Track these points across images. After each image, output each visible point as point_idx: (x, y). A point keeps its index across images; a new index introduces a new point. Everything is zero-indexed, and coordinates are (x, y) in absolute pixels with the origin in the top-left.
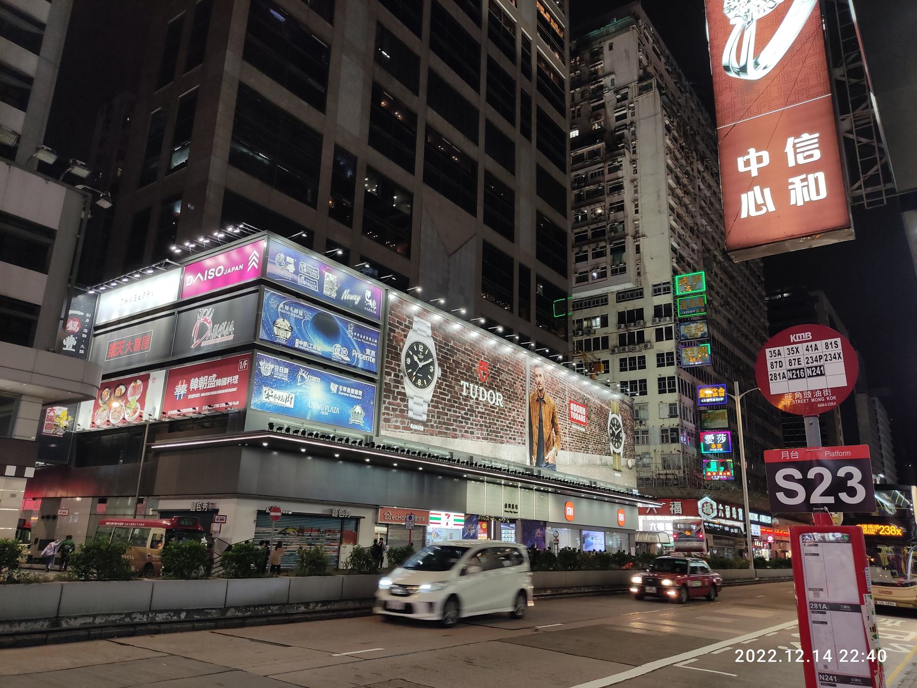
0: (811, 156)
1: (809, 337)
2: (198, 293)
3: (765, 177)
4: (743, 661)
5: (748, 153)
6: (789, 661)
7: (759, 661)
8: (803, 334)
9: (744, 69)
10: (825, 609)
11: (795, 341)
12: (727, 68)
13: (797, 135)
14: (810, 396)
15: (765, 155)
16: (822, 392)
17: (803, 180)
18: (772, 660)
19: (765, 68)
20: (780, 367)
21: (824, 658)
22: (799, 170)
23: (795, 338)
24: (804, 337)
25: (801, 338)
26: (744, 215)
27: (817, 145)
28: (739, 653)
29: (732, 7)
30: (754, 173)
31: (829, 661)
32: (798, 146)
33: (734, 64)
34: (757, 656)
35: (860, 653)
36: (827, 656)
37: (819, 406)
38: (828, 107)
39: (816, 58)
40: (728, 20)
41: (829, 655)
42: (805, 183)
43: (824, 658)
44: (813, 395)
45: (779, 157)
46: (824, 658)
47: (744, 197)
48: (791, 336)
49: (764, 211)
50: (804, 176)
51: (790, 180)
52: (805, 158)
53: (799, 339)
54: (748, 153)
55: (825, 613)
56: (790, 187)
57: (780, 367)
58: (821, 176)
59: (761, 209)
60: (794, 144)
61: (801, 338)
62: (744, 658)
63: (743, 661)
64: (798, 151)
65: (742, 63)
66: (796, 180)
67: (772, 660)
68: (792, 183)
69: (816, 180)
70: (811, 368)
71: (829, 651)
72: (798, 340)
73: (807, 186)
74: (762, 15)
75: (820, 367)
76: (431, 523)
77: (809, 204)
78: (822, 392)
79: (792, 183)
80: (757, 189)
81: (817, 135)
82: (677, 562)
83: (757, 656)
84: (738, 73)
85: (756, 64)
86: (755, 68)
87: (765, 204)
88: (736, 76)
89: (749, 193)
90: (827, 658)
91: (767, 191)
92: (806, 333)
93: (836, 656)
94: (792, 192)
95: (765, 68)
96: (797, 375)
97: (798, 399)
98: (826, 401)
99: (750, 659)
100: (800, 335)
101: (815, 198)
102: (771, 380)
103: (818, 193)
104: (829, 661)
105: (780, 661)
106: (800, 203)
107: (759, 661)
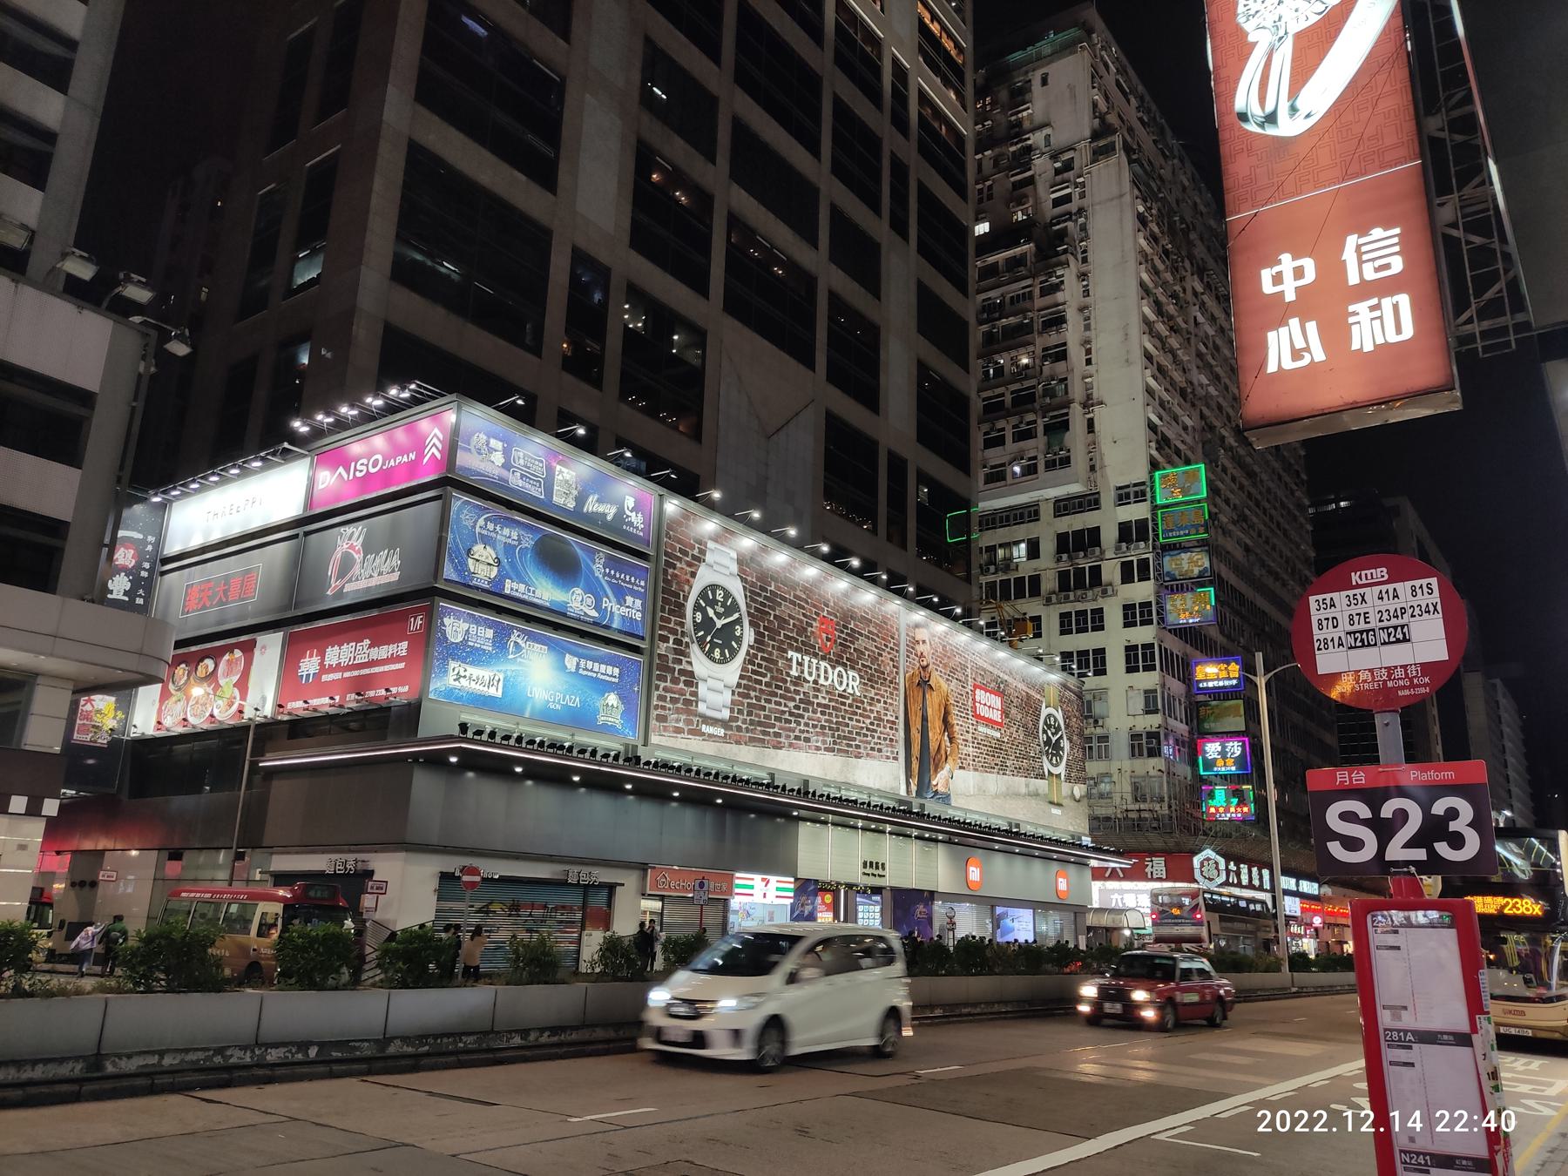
0: (1387, 266)
1: (1383, 576)
3: (1308, 302)
4: (1270, 1130)
5: (1279, 262)
6: (1350, 1129)
7: (1298, 1129)
8: (1373, 571)
9: (1271, 118)
10: (1410, 1041)
11: (1360, 582)
12: (1243, 117)
13: (1363, 232)
14: (1384, 678)
15: (1309, 264)
16: (1406, 671)
17: (1373, 308)
18: (1320, 1127)
19: (1308, 116)
20: (1334, 627)
21: (1410, 1125)
22: (1367, 290)
23: (1360, 577)
24: (1375, 577)
25: (1369, 577)
26: (1272, 367)
27: (1397, 249)
28: (1264, 1116)
29: (1252, 12)
30: (1290, 296)
31: (1418, 1130)
32: (1364, 249)
33: (1256, 110)
34: (1295, 1122)
35: (1470, 1117)
36: (1414, 1122)
37: (1400, 693)
38: (1416, 182)
39: (1395, 99)
40: (1245, 34)
41: (1418, 1120)
42: (1377, 313)
43: (1410, 1125)
44: (1389, 675)
45: (1332, 269)
46: (1410, 1125)
47: (1272, 336)
48: (1353, 574)
49: (1306, 361)
50: (1374, 301)
51: (1351, 308)
52: (1377, 270)
53: (1367, 579)
54: (1279, 262)
55: (1410, 1048)
56: (1351, 320)
57: (1334, 627)
58: (1404, 300)
59: (1302, 357)
60: (1359, 247)
61: (1369, 577)
62: (1272, 1124)
63: (1270, 1130)
64: (1365, 257)
65: (1269, 108)
66: (1362, 308)
67: (1320, 1127)
68: (1355, 314)
69: (1396, 307)
70: (1388, 628)
71: (1417, 1113)
72: (1364, 581)
73: (1381, 318)
74: (1303, 25)
75: (1403, 627)
76: (737, 894)
77: (1384, 349)
78: (1406, 671)
79: (1355, 314)
80: (1294, 323)
81: (1397, 231)
83: (1295, 1122)
84: (1261, 125)
85: (1293, 110)
86: (1292, 116)
87: (1307, 349)
88: (1259, 130)
89: (1281, 330)
90: (1414, 1125)
91: (1312, 327)
92: (1379, 570)
93: (1430, 1122)
94: (1355, 329)
95: (1308, 116)
97: (1365, 681)
98: (1412, 686)
99: (1283, 1126)
100: (1368, 572)
101: (1393, 338)
102: (1319, 649)
103: (1399, 330)
104: (1418, 1130)
105: (1334, 1130)
106: (1369, 347)
107: (1298, 1129)
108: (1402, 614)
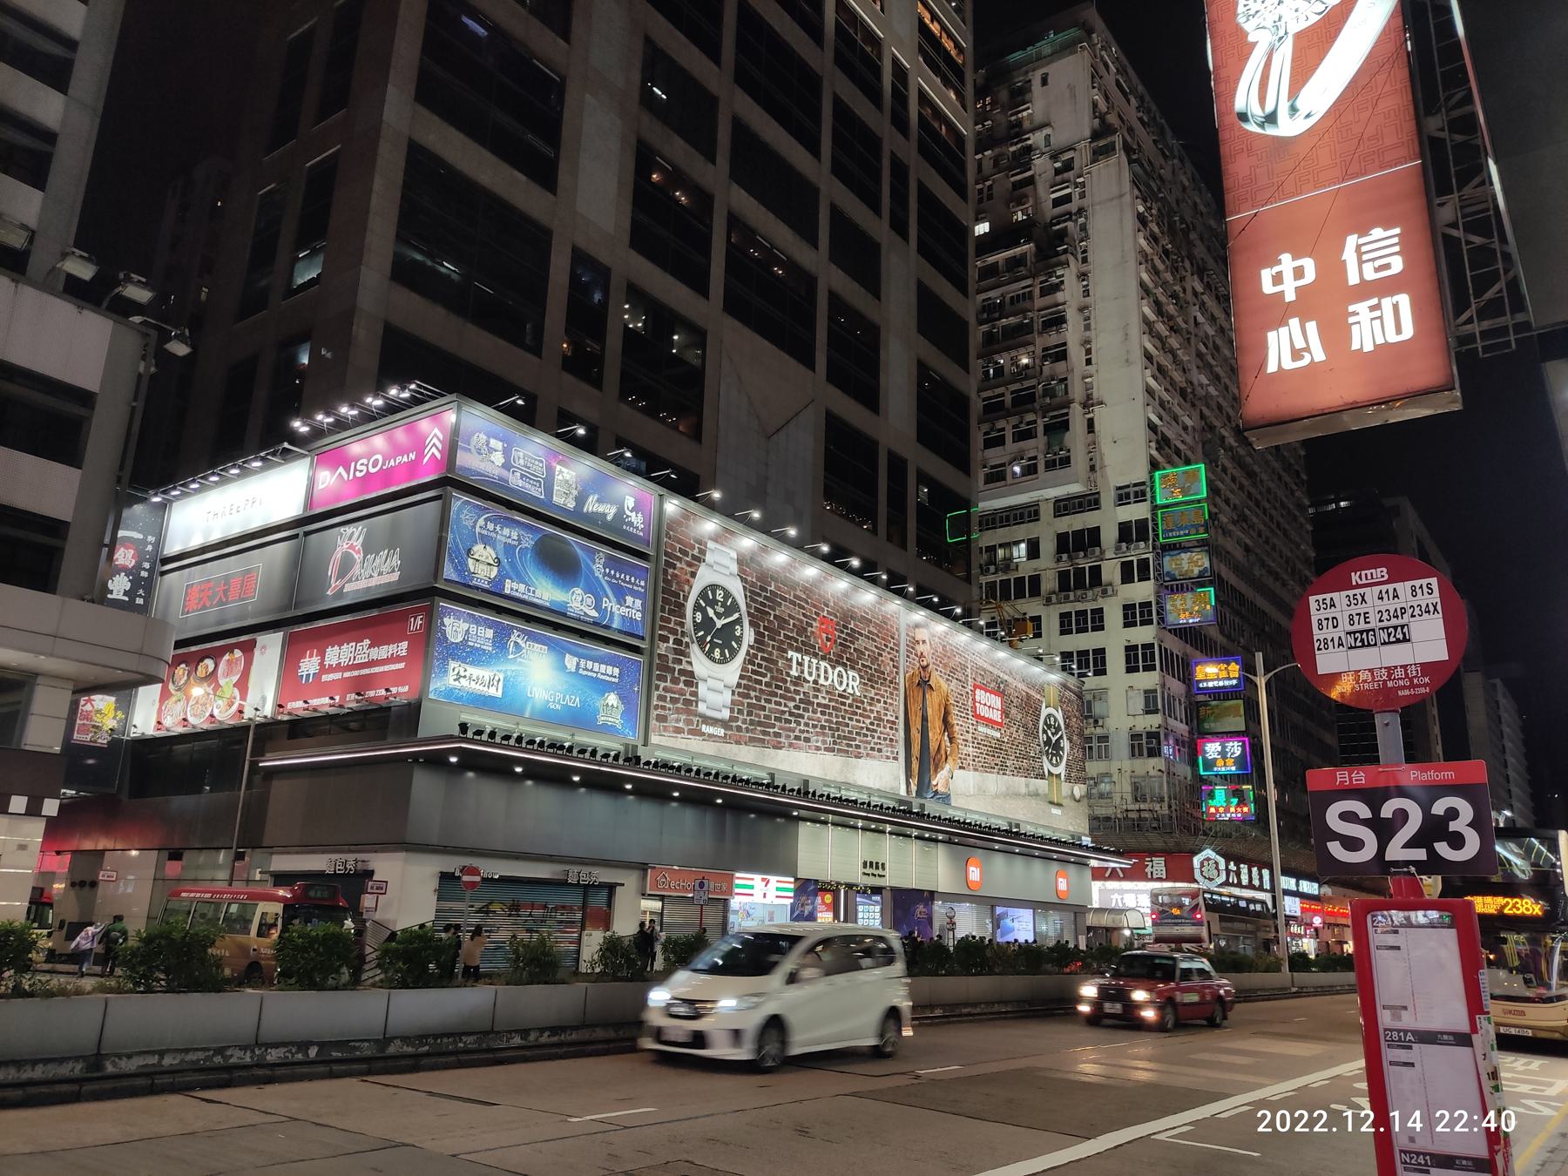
0: (1387, 266)
1: (1383, 576)
2: (338, 500)
3: (1308, 302)
4: (1270, 1130)
5: (1279, 262)
6: (1350, 1129)
7: (1298, 1129)
8: (1373, 571)
9: (1271, 118)
10: (1410, 1041)
11: (1360, 582)
12: (1243, 117)
13: (1363, 232)
14: (1384, 678)
15: (1309, 264)
16: (1406, 671)
17: (1373, 308)
18: (1320, 1127)
19: (1308, 116)
20: (1334, 627)
21: (1410, 1125)
22: (1367, 290)
23: (1360, 577)
24: (1375, 577)
25: (1369, 577)
26: (1272, 367)
27: (1397, 249)
28: (1264, 1116)
29: (1252, 12)
30: (1290, 296)
31: (1418, 1130)
32: (1364, 249)
33: (1256, 110)
34: (1295, 1122)
35: (1470, 1117)
36: (1414, 1122)
38: (1416, 182)
39: (1395, 99)
40: (1245, 34)
41: (1418, 1120)
42: (1377, 313)
43: (1410, 1125)
44: (1389, 675)
45: (1332, 269)
46: (1410, 1125)
47: (1272, 336)
48: (1353, 574)
49: (1306, 361)
50: (1374, 301)
51: (1351, 308)
52: (1377, 270)
53: (1367, 579)
54: (1279, 262)
55: (1410, 1048)
56: (1351, 320)
57: (1334, 627)
58: (1404, 300)
59: (1302, 357)
60: (1359, 247)
61: (1369, 577)
62: (1272, 1124)
63: (1270, 1130)
64: (1365, 257)
65: (1269, 108)
66: (1362, 308)
67: (1320, 1127)
68: (1355, 314)
69: (1396, 307)
70: (1388, 628)
71: (1417, 1113)
72: (1364, 581)
73: (1381, 318)
74: (1303, 25)
75: (1403, 627)
76: (737, 894)
77: (1384, 349)
78: (1406, 671)
79: (1355, 314)
80: (1294, 323)
81: (1397, 231)
82: (1157, 961)
83: (1295, 1122)
84: (1261, 125)
85: (1293, 110)
86: (1292, 116)
87: (1307, 349)
88: (1259, 130)
89: (1281, 330)
90: (1414, 1125)
91: (1312, 327)
92: (1379, 570)
93: (1430, 1122)
94: (1355, 329)
95: (1308, 116)
96: (1362, 641)
97: (1365, 681)
99: (1283, 1126)
100: (1368, 572)
101: (1393, 338)
102: (1319, 649)
103: (1399, 330)
104: (1418, 1130)
105: (1334, 1130)
106: (1369, 347)
107: (1298, 1129)
108: (1402, 614)
